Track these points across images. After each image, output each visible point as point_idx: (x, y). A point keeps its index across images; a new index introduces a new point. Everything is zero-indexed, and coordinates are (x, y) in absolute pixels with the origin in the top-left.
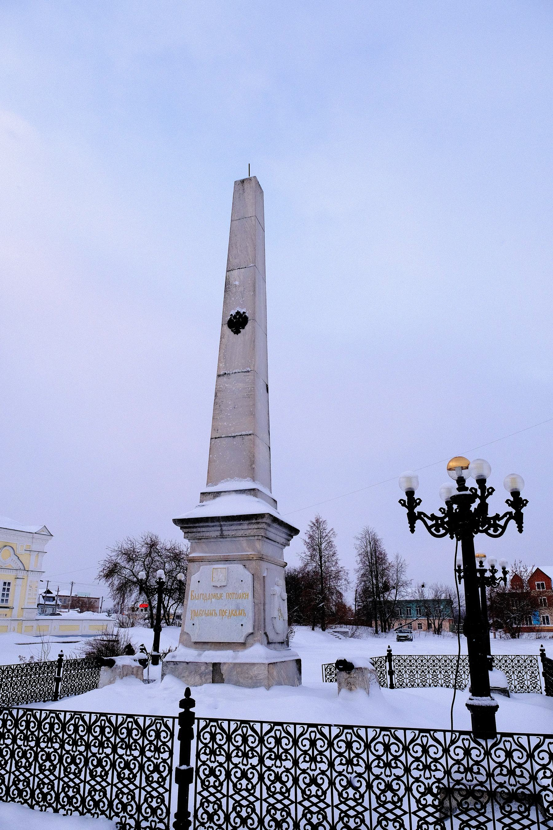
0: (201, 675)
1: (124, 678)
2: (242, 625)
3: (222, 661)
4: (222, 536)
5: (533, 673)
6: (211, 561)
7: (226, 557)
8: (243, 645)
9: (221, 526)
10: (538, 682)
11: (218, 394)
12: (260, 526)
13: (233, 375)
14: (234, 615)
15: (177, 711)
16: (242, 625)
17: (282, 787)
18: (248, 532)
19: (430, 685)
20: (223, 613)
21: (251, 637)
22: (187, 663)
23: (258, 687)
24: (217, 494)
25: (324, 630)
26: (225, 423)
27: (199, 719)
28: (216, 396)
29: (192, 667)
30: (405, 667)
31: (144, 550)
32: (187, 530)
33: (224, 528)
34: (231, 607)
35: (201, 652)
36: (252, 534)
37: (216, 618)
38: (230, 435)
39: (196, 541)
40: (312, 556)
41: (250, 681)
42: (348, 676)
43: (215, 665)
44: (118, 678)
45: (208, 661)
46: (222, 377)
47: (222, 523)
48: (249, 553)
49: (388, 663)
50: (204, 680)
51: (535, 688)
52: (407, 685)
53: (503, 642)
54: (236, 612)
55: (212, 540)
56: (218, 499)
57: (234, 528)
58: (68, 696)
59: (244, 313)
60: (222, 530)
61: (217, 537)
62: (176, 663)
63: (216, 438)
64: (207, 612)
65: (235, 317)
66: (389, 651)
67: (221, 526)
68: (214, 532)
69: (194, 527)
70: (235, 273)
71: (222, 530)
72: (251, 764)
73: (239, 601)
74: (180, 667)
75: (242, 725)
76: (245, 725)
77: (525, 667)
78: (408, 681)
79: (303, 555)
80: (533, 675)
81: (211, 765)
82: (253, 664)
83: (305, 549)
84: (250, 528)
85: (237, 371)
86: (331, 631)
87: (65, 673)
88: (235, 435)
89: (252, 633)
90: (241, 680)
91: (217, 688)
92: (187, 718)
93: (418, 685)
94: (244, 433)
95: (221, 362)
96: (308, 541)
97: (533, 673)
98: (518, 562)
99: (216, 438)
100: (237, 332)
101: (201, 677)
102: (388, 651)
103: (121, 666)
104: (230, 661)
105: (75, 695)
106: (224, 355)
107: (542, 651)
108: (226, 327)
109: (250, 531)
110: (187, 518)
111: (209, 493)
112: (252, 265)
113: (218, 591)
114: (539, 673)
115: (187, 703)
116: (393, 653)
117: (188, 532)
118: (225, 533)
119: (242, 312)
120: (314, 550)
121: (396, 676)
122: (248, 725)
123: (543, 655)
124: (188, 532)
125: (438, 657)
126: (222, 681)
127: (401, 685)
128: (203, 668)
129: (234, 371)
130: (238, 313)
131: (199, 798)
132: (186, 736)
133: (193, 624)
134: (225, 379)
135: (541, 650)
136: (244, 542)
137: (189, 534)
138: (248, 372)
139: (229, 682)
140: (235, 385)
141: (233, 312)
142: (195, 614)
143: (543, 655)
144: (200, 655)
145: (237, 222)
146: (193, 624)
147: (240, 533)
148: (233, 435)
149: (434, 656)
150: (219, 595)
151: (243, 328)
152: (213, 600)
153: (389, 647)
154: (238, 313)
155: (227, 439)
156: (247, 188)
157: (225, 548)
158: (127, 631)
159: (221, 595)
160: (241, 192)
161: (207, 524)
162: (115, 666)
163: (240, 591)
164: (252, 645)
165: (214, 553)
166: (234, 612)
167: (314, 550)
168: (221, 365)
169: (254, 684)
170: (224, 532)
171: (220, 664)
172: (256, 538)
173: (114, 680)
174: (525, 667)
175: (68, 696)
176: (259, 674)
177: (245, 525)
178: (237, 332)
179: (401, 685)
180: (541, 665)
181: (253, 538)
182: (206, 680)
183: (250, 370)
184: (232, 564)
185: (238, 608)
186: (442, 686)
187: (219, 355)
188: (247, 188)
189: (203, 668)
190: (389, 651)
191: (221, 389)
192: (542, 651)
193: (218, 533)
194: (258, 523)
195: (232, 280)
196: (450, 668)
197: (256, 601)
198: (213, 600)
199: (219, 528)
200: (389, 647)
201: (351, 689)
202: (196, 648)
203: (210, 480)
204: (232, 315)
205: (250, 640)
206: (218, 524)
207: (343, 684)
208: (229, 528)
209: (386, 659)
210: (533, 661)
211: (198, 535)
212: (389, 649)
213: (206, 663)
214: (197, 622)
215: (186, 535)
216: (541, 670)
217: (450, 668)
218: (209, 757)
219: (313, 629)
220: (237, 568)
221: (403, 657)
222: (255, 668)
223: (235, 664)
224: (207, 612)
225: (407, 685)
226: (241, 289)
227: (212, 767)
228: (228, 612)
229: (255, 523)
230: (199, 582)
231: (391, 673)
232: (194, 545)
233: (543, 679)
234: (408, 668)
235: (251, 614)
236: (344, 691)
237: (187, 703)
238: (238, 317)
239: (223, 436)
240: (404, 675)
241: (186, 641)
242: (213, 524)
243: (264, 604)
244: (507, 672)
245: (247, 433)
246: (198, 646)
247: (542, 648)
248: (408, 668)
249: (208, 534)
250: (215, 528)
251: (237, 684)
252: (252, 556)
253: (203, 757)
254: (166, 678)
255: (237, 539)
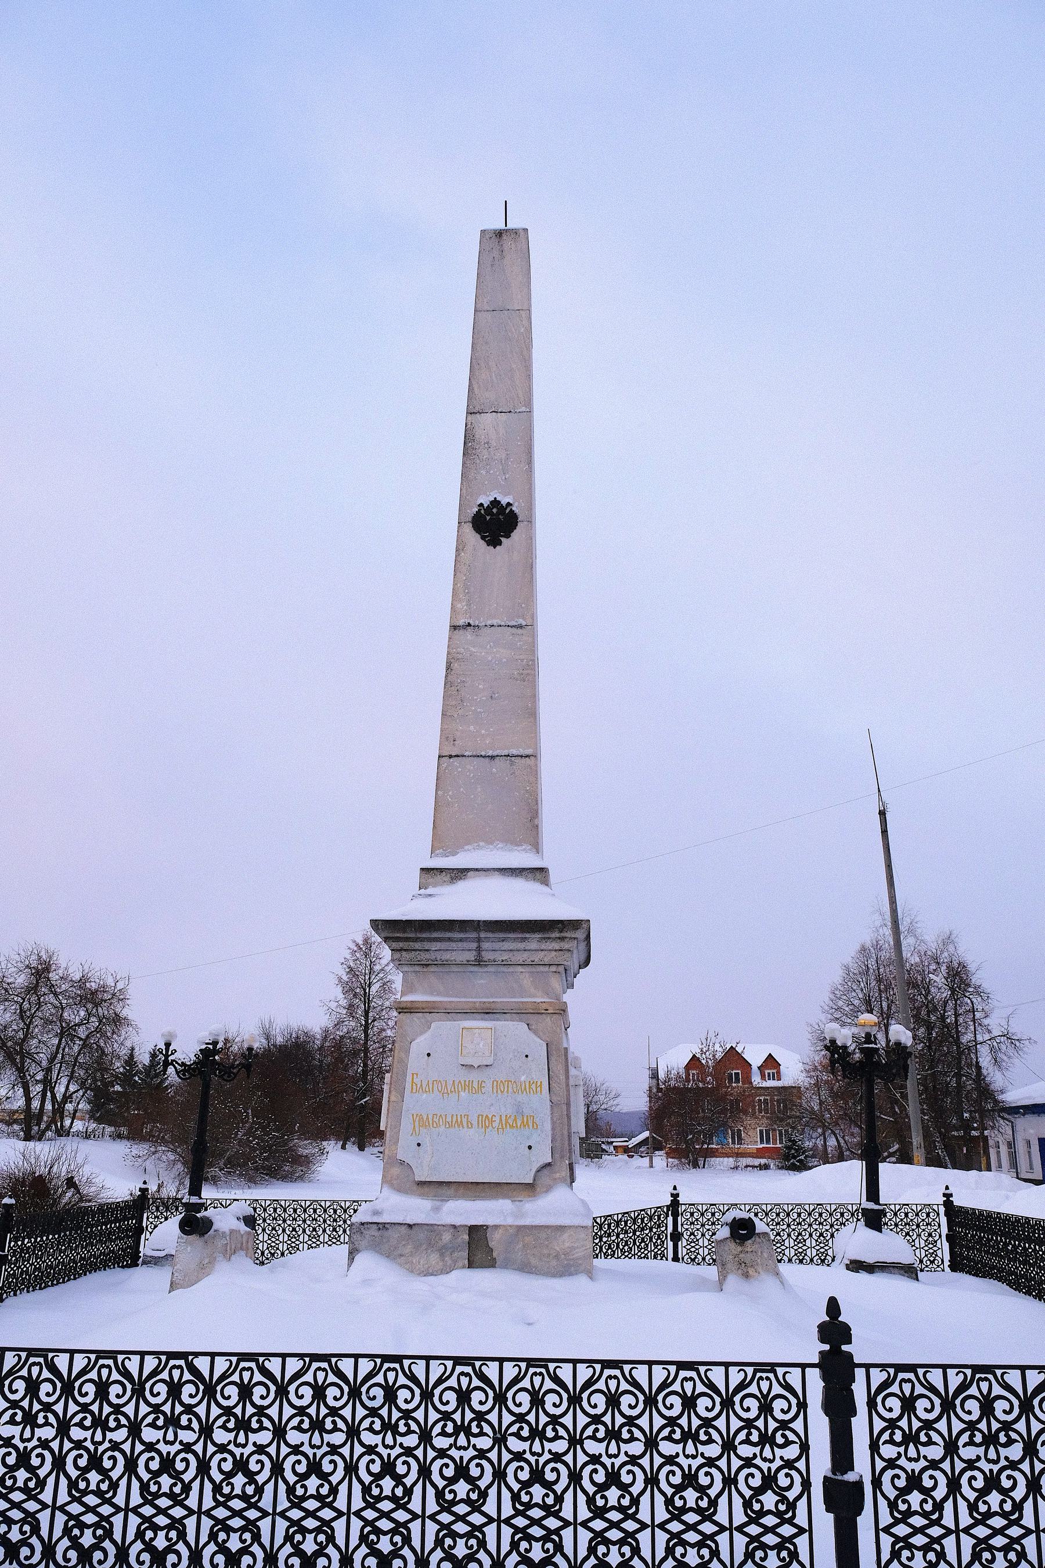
0: (442, 1251)
1: (233, 1258)
2: (530, 1147)
3: (490, 1222)
4: (479, 962)
5: (930, 1235)
6: (451, 1012)
7: (484, 1006)
8: (530, 1188)
9: (479, 940)
10: (939, 1253)
11: (455, 665)
12: (566, 945)
13: (488, 630)
14: (512, 1127)
15: (812, 1350)
16: (530, 1147)
17: (1003, 1501)
18: (537, 957)
19: (790, 1260)
20: (485, 1122)
21: (545, 1171)
22: (410, 1226)
23: (571, 1274)
24: (459, 874)
25: (362, 1148)
26: (472, 728)
27: (867, 1367)
28: (449, 668)
29: (422, 1235)
30: (703, 1225)
31: (21, 980)
32: (395, 945)
33: (485, 945)
34: (503, 1109)
35: (438, 1203)
36: (546, 960)
37: (471, 1132)
38: (483, 753)
39: (417, 968)
40: (351, 1007)
41: (554, 1263)
42: (739, 1249)
43: (473, 1230)
44: (220, 1258)
45: (458, 1221)
46: (461, 632)
47: (483, 935)
48: (539, 1000)
49: (670, 1219)
50: (449, 1262)
51: (932, 1262)
52: (704, 1259)
53: (679, 1174)
54: (515, 1120)
55: (455, 969)
56: (461, 885)
57: (507, 945)
58: (15, 1295)
59: (509, 504)
60: (479, 949)
61: (468, 963)
62: (383, 1226)
63: (451, 757)
64: (449, 1119)
65: (488, 510)
66: (675, 1196)
67: (479, 940)
68: (461, 952)
69: (416, 940)
70: (488, 419)
71: (479, 949)
72: (1007, 1458)
73: (521, 1097)
74: (393, 1234)
75: (978, 1376)
76: (983, 1376)
77: (918, 1226)
78: (706, 1251)
79: (333, 1005)
80: (931, 1239)
81: (909, 1466)
82: (561, 1228)
83: (338, 993)
84: (543, 947)
85: (495, 622)
86: (376, 1150)
87: (13, 1244)
88: (495, 754)
89: (549, 1164)
90: (534, 1261)
91: (483, 1278)
92: (837, 1367)
93: (812, 1260)
94: (515, 752)
95: (460, 601)
96: (345, 978)
97: (930, 1235)
98: (711, 1035)
99: (451, 757)
100: (494, 542)
101: (442, 1255)
102: (672, 1195)
103: (228, 1232)
104: (510, 1221)
105: (28, 1292)
106: (466, 587)
107: (948, 1196)
108: (468, 528)
109: (543, 953)
110: (404, 918)
111: (441, 870)
112: (523, 409)
113: (474, 1077)
114: (940, 1236)
115: (834, 1331)
116: (681, 1200)
117: (401, 950)
118: (487, 956)
119: (504, 502)
120: (355, 995)
121: (685, 1243)
122: (990, 1377)
123: (948, 1203)
124: (401, 950)
125: (764, 1207)
126: (491, 1263)
127: (693, 1260)
128: (447, 1237)
129: (489, 623)
130: (495, 503)
131: (886, 1541)
132: (838, 1407)
133: (419, 1145)
134: (469, 635)
135: (944, 1195)
136: (525, 978)
137: (404, 953)
138: (521, 627)
139: (505, 1266)
140: (489, 650)
141: (486, 501)
142: (422, 1122)
143: (948, 1203)
144: (437, 1209)
145: (489, 315)
146: (419, 1145)
147: (521, 957)
148: (490, 753)
149: (757, 1205)
150: (475, 1085)
151: (508, 536)
152: (462, 1094)
153: (675, 1188)
154: (495, 503)
155: (476, 760)
156: (503, 244)
157: (483, 987)
158: (68, 1149)
159: (481, 1085)
160: (496, 253)
161: (448, 935)
162: (211, 1232)
163: (523, 1078)
164: (548, 1189)
165: (465, 997)
166: (510, 1121)
167: (355, 995)
168: (459, 606)
169: (566, 1268)
170: (483, 953)
171: (487, 1226)
172: (553, 969)
173: (212, 1262)
174: (918, 1226)
175: (15, 1295)
176: (572, 1248)
177: (533, 942)
178: (494, 542)
179: (693, 1260)
180: (944, 1220)
181: (546, 969)
182: (455, 1262)
183: (524, 623)
184: (498, 1020)
185: (519, 1112)
186: (790, 1260)
187: (455, 584)
188: (503, 244)
189: (447, 1237)
190: (675, 1196)
191: (460, 656)
192: (948, 1196)
193: (471, 956)
194: (562, 939)
195: (479, 434)
196: (785, 1227)
197: (555, 1099)
198: (462, 1094)
199: (474, 945)
200: (947, 1188)
201: (746, 1276)
202: (422, 1195)
203: (439, 843)
204: (481, 505)
205: (545, 1179)
206: (474, 935)
207: (729, 1266)
208: (497, 945)
209: (668, 1210)
210: (931, 1215)
211: (424, 956)
212: (675, 1192)
213: (454, 1227)
214: (426, 1142)
215: (397, 955)
216: (944, 1230)
217: (785, 1227)
218: (902, 1449)
219: (343, 1147)
220: (515, 1030)
221: (700, 1208)
222: (566, 1236)
223: (520, 1228)
224: (449, 1119)
225: (704, 1259)
226: (501, 455)
227: (913, 1471)
228: (497, 1119)
229: (515, 939)
230: (429, 1055)
231: (676, 1237)
232: (412, 977)
233: (946, 1246)
234: (707, 1227)
235: (548, 1126)
236: (733, 1280)
237: (834, 1331)
238: (495, 510)
239: (467, 754)
240: (701, 1241)
241: (404, 1179)
242: (462, 935)
243: (568, 1104)
244: (907, 1234)
245: (521, 752)
246: (426, 1189)
247: (947, 1192)
248: (707, 1227)
249: (447, 956)
250: (465, 945)
251: (526, 1268)
252: (544, 1006)
253: (889, 1451)
254: (359, 1258)
255: (511, 969)
